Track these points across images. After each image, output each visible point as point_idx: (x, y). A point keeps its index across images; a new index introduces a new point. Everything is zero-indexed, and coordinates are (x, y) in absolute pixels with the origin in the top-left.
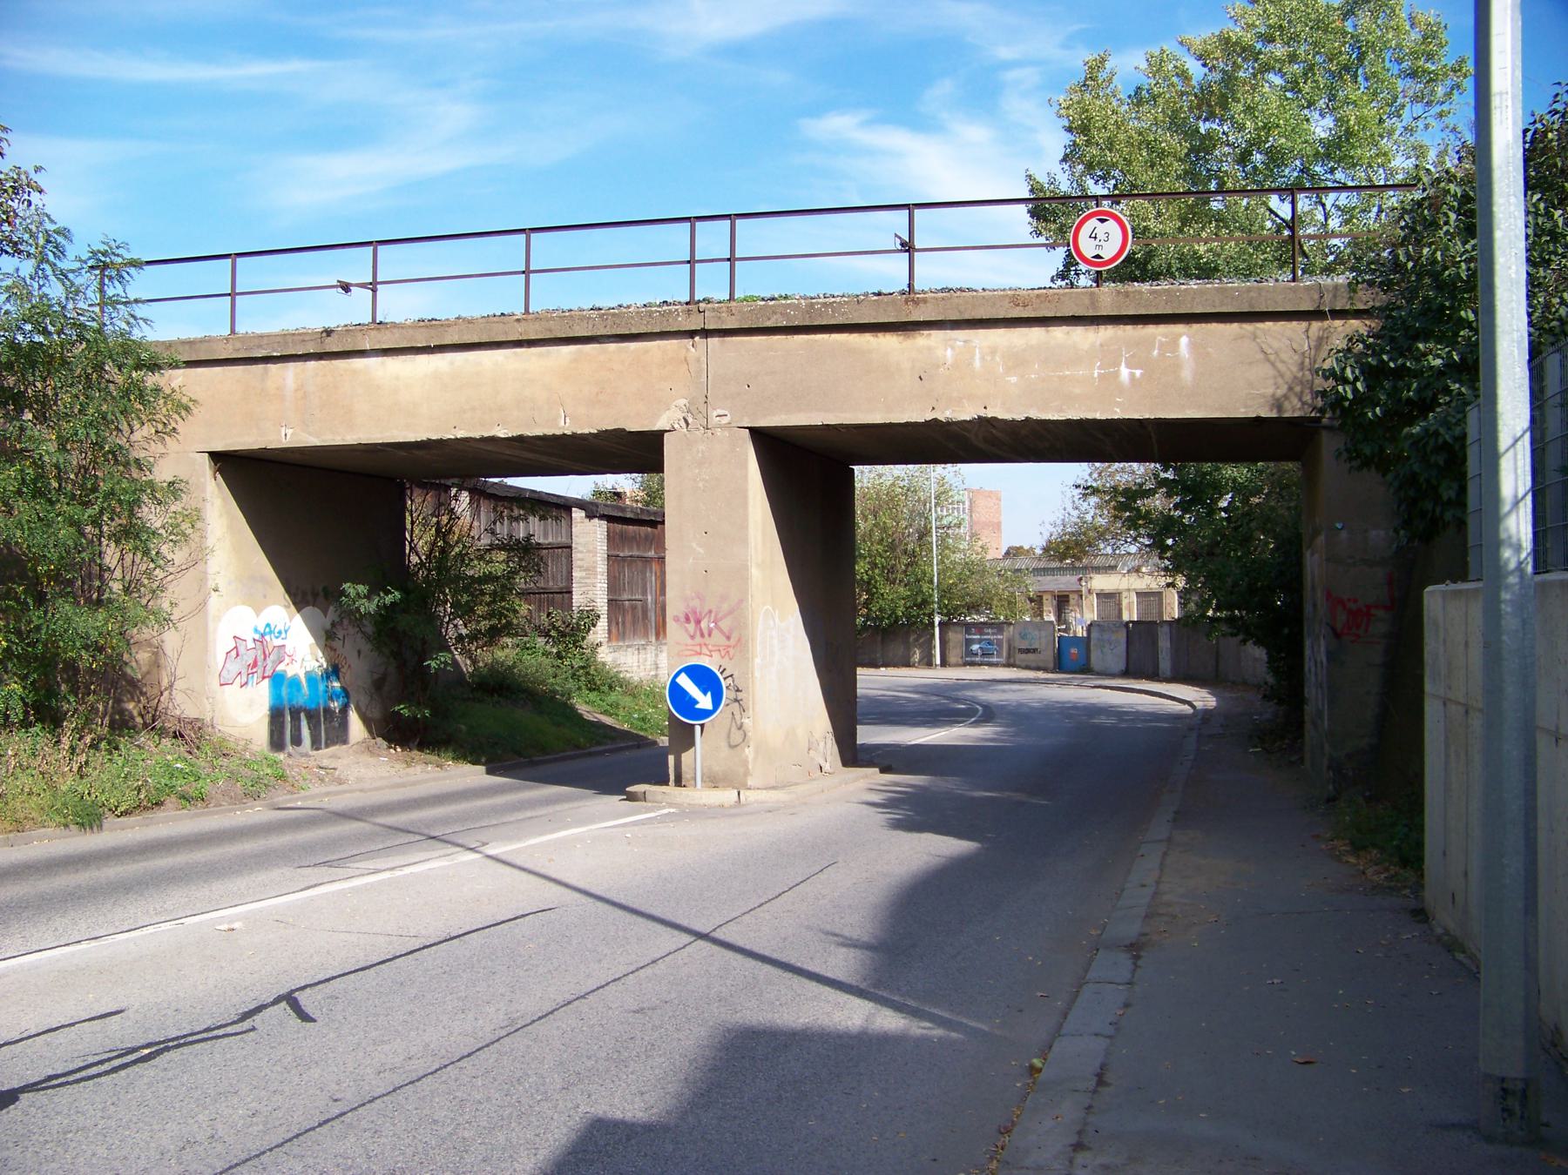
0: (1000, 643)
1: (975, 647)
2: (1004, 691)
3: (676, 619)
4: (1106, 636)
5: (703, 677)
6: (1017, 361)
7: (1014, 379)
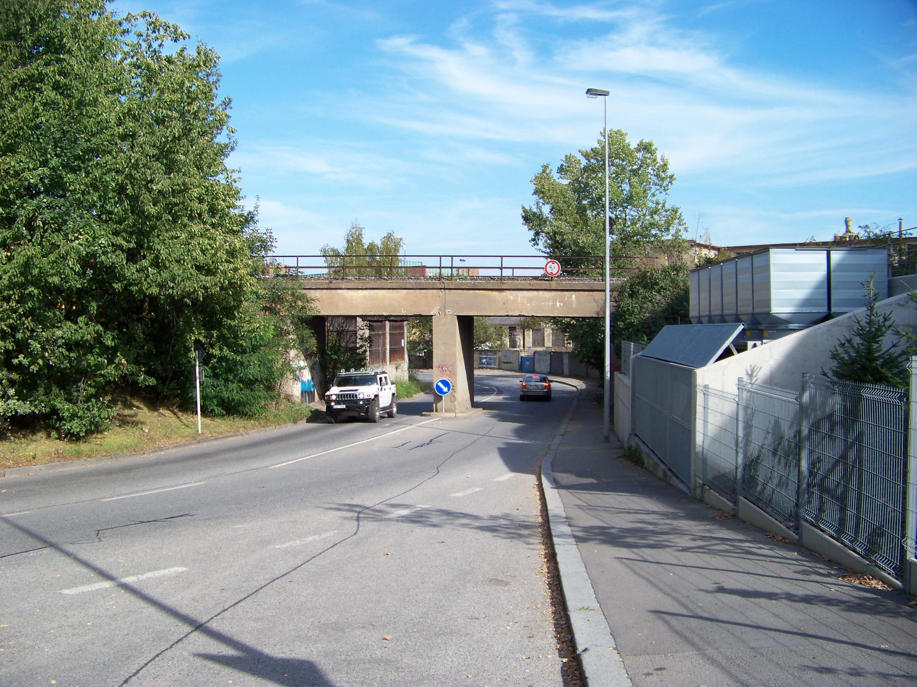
0: (495, 359)
1: (484, 361)
2: (501, 381)
3: (436, 367)
4: (542, 357)
5: (445, 383)
6: (530, 300)
7: (529, 305)
